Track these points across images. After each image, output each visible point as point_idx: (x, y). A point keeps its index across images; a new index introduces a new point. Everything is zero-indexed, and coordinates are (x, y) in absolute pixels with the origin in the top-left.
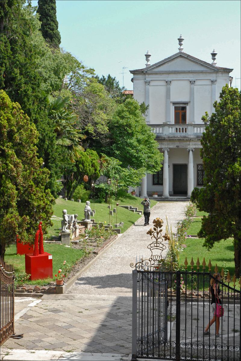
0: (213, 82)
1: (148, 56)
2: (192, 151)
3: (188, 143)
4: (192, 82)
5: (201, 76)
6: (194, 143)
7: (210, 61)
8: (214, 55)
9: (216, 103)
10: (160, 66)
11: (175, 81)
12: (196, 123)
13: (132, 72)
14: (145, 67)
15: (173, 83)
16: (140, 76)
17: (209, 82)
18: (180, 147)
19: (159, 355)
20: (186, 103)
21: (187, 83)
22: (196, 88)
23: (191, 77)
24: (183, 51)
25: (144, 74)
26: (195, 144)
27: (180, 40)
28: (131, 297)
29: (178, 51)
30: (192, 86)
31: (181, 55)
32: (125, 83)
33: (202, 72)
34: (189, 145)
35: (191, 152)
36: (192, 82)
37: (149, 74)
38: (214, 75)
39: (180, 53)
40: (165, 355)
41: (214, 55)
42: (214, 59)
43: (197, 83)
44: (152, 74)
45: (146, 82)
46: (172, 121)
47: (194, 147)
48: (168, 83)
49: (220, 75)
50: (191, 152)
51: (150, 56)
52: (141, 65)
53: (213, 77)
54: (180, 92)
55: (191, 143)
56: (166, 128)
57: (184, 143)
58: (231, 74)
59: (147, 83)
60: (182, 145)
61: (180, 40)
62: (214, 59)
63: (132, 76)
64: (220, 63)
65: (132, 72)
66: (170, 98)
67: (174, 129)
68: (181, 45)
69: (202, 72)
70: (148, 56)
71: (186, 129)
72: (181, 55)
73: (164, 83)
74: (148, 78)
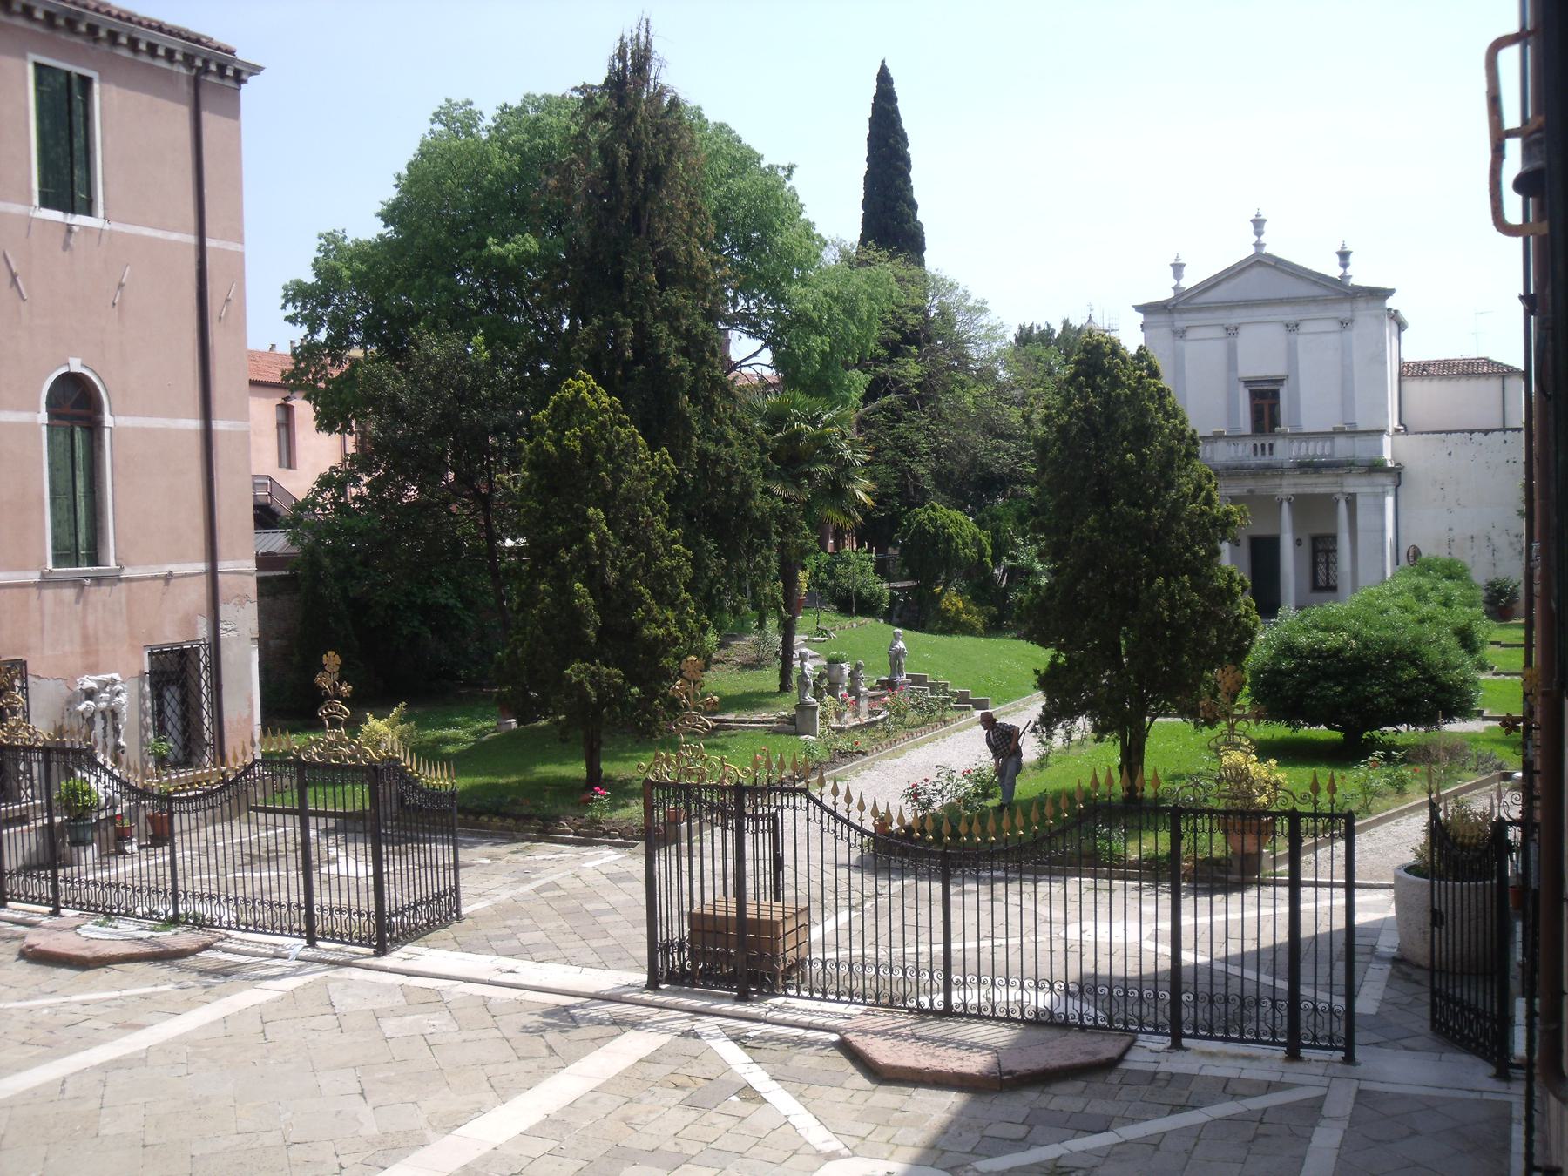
0: (1345, 324)
1: (1178, 268)
2: (1289, 501)
3: (1277, 481)
4: (1292, 327)
5: (1314, 310)
6: (1292, 481)
7: (1334, 271)
8: (1344, 256)
9: (471, 103)
10: (1213, 286)
11: (1508, 408)
12: (1306, 430)
13: (1139, 308)
14: (1170, 294)
15: (1243, 331)
16: (1160, 318)
17: (1335, 326)
18: (1258, 492)
19: (1257, 1034)
20: (1279, 381)
21: (1281, 329)
22: (1300, 339)
23: (1289, 314)
24: (1267, 250)
25: (1170, 312)
26: (1295, 485)
27: (1258, 224)
28: (578, 780)
29: (1252, 251)
30: (1292, 335)
31: (1261, 262)
32: (1131, 338)
33: (1314, 300)
34: (1280, 486)
35: (1285, 505)
36: (1292, 327)
37: (1182, 311)
38: (1347, 306)
39: (1257, 254)
40: (1257, 1034)
41: (1344, 256)
42: (1344, 265)
43: (1304, 328)
44: (1189, 310)
45: (1175, 332)
46: (1245, 423)
47: (1294, 491)
48: (1232, 331)
49: (1361, 304)
50: (1285, 505)
51: (1183, 265)
52: (1165, 293)
53: (1344, 311)
54: (1261, 351)
55: (1285, 482)
56: (1221, 445)
57: (1268, 482)
58: (1390, 303)
59: (1180, 334)
60: (1262, 486)
61: (1258, 224)
62: (1344, 265)
63: (1140, 317)
64: (1360, 276)
65: (1139, 308)
66: (1236, 370)
67: (1250, 446)
68: (1259, 233)
69: (1314, 300)
70: (1178, 268)
71: (1271, 446)
72: (1261, 262)
73: (1220, 333)
74: (1181, 321)
